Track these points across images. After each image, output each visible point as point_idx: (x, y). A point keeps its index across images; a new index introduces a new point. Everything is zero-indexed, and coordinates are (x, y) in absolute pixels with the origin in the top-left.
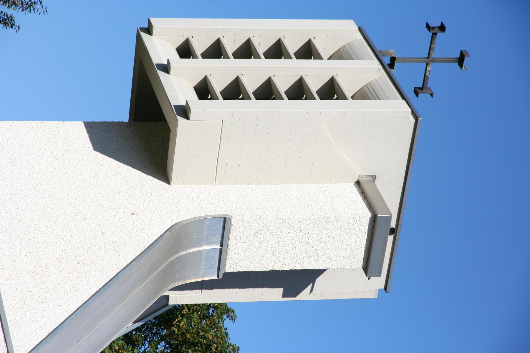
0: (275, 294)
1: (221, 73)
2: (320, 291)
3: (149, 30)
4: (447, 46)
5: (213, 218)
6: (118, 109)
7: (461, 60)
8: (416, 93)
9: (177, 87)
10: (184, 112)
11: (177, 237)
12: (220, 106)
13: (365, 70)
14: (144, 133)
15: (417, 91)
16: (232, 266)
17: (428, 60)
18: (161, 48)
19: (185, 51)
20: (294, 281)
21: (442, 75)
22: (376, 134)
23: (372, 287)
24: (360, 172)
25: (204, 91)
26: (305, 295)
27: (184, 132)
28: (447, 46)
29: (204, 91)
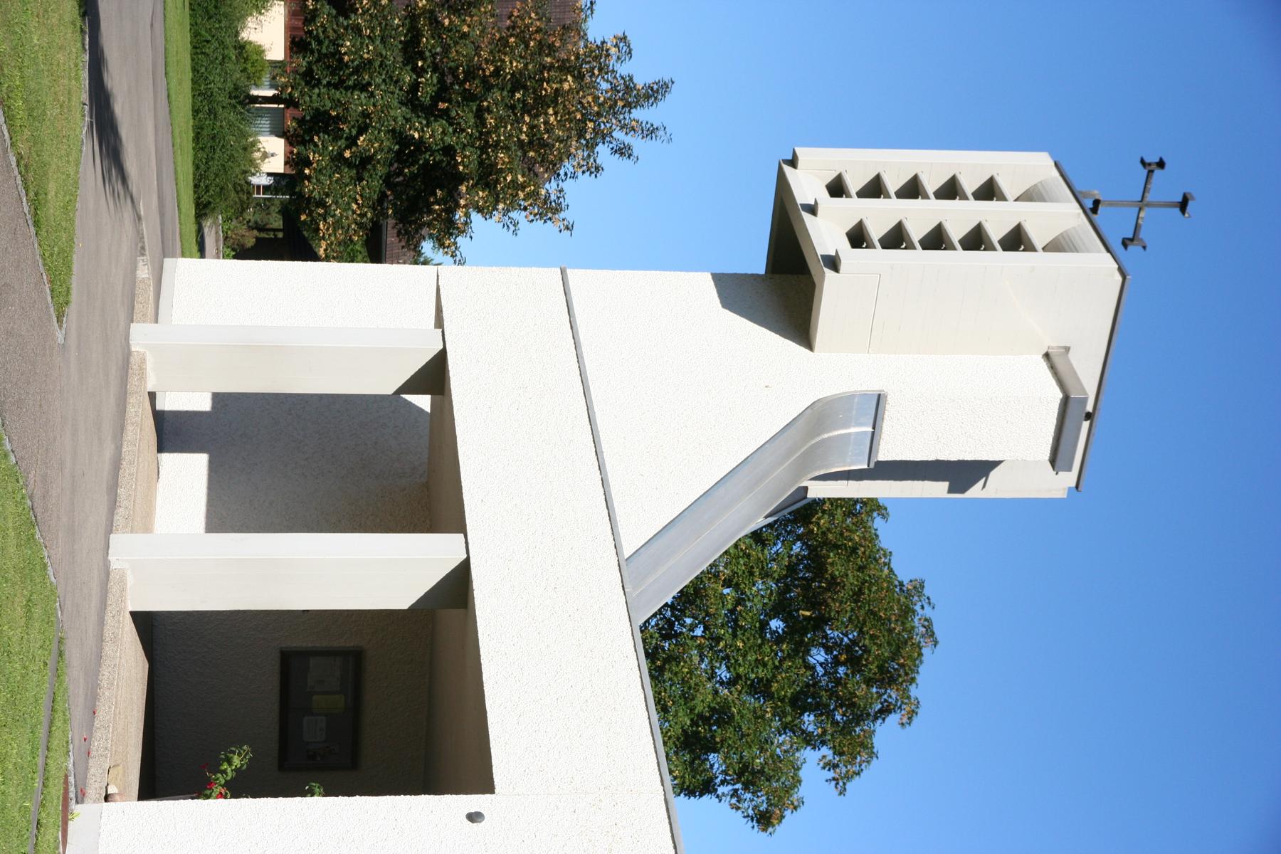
0: (938, 489)
3: (793, 163)
4: (1166, 187)
5: (865, 395)
6: (753, 258)
7: (1183, 205)
9: (825, 232)
11: (819, 416)
12: (877, 257)
13: (1062, 215)
14: (784, 288)
16: (886, 453)
17: (1142, 204)
18: (807, 186)
19: (837, 188)
20: (964, 474)
21: (1158, 223)
22: (1070, 296)
24: (1051, 342)
25: (858, 238)
26: (975, 492)
27: (832, 288)
28: (1166, 187)
29: (858, 238)
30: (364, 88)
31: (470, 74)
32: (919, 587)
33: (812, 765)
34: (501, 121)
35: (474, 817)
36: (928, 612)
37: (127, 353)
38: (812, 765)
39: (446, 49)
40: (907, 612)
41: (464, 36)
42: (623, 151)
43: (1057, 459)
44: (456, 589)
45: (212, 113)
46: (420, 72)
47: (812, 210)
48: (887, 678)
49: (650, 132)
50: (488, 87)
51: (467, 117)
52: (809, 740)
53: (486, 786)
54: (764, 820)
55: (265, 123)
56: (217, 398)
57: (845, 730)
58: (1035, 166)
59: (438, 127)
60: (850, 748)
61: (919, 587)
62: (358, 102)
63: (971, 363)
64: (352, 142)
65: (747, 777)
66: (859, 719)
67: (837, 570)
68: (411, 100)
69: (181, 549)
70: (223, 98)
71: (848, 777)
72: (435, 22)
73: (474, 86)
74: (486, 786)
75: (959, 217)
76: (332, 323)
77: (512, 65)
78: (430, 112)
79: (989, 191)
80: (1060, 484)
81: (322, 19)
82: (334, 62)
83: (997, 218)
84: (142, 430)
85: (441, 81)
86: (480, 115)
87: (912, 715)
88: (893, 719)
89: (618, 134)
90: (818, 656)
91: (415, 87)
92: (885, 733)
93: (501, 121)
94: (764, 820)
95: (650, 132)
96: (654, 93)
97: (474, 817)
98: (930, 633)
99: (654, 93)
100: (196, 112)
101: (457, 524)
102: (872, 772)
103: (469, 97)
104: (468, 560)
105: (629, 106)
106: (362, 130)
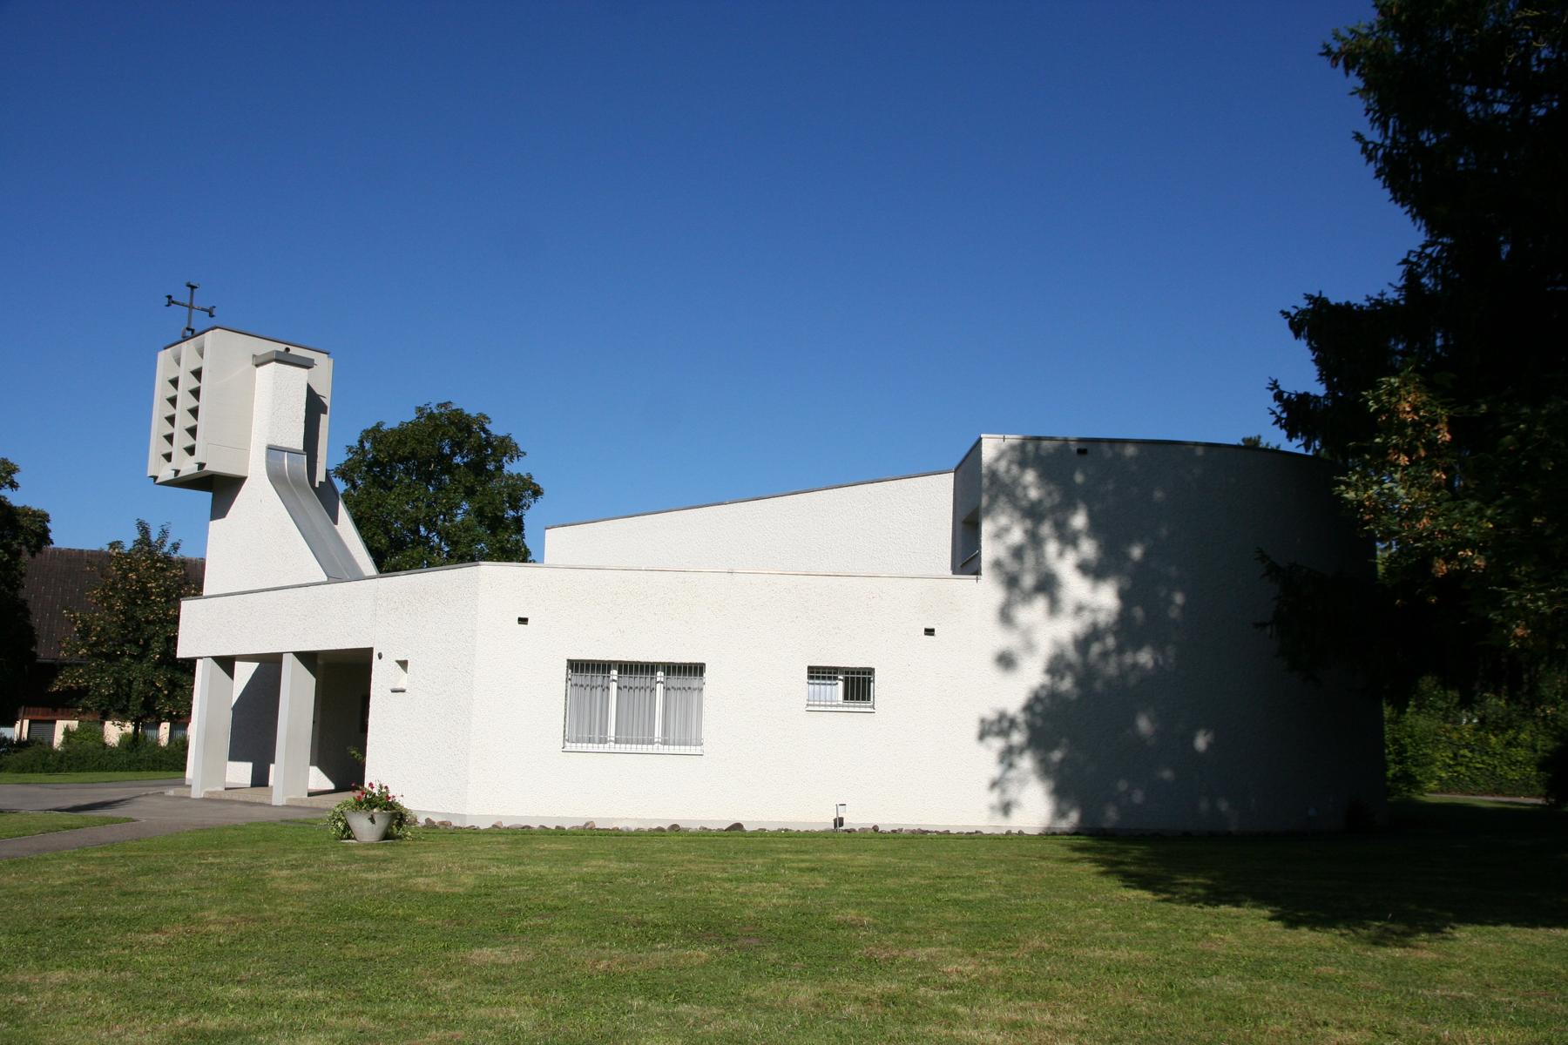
0: (324, 420)
1: (182, 440)
2: (324, 391)
3: (155, 478)
4: (182, 295)
5: (267, 455)
6: (206, 497)
7: (193, 287)
8: (213, 318)
9: (188, 467)
10: (201, 466)
11: (276, 478)
12: (200, 443)
13: (187, 348)
14: (221, 489)
15: (211, 316)
16: (298, 444)
17: (191, 307)
18: (166, 473)
19: (168, 457)
20: (314, 406)
21: (201, 299)
22: (224, 352)
23: (324, 363)
24: (250, 364)
25: (191, 451)
26: (327, 401)
27: (211, 467)
28: (182, 295)
29: (191, 451)
30: (130, 683)
31: (124, 626)
32: (420, 410)
33: (512, 468)
34: (153, 612)
35: (380, 656)
36: (433, 406)
37: (203, 799)
38: (512, 468)
39: (111, 639)
40: (431, 416)
41: (103, 629)
42: (176, 547)
43: (307, 364)
44: (308, 659)
45: (140, 761)
46: (123, 653)
47: (177, 472)
48: (468, 429)
49: (164, 533)
50: (133, 617)
51: (151, 629)
52: (500, 468)
53: (370, 650)
54: (537, 492)
55: (150, 733)
56: (235, 756)
57: (494, 449)
58: (164, 357)
59: (154, 645)
60: (506, 448)
61: (420, 410)
62: (138, 686)
63: (257, 402)
64: (159, 690)
65: (516, 503)
66: (489, 444)
67: (407, 450)
68: (139, 658)
69: (297, 778)
70: (133, 756)
71: (517, 449)
72: (95, 644)
73: (131, 626)
74: (370, 650)
75: (186, 401)
76: (212, 704)
77: (119, 605)
78: (146, 647)
79: (175, 382)
80: (324, 363)
81: (89, 703)
82: (113, 699)
83: (188, 383)
84: (258, 794)
85: (129, 642)
86: (148, 622)
87: (486, 418)
88: (487, 426)
89: (165, 550)
90: (458, 460)
91: (131, 656)
92: (497, 429)
93: (153, 612)
94: (537, 492)
95: (164, 533)
96: (144, 529)
97: (380, 656)
98: (445, 405)
99: (144, 529)
100: (139, 770)
101: (280, 655)
102: (515, 438)
103: (138, 628)
104: (215, 658)
105: (149, 544)
106: (153, 684)
